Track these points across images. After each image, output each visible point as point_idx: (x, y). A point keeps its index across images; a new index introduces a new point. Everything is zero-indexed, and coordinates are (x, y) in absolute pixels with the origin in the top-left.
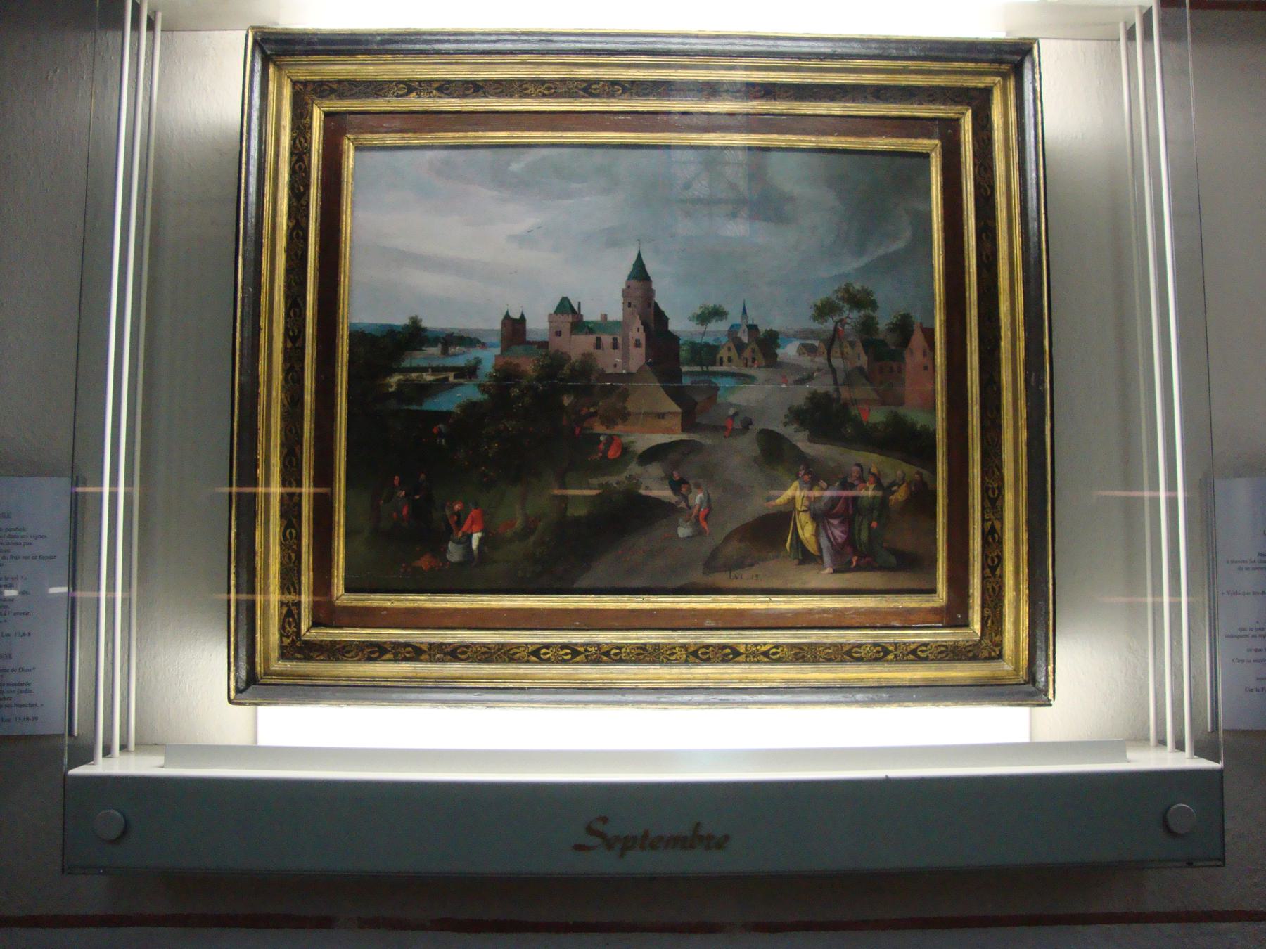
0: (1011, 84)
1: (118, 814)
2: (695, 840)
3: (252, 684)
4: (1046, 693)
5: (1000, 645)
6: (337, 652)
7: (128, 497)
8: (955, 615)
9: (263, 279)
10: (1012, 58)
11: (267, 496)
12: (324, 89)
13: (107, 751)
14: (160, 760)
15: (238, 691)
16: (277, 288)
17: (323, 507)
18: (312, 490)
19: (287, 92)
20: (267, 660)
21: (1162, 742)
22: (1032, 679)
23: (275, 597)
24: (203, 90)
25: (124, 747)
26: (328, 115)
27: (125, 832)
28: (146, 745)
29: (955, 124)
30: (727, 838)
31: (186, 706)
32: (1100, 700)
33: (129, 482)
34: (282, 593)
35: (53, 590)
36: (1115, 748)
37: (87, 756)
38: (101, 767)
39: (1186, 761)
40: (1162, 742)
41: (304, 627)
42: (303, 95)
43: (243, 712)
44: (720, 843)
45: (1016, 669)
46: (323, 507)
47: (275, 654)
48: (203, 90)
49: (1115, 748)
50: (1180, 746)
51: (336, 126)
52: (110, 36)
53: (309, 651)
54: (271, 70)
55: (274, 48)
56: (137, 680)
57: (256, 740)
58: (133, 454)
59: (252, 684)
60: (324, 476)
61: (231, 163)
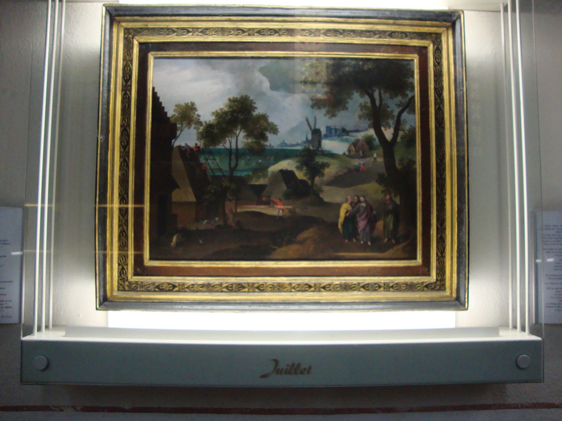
0: (450, 32)
1: (45, 358)
2: (295, 369)
3: (105, 302)
4: (464, 306)
5: (444, 285)
6: (146, 288)
7: (50, 209)
8: (425, 270)
9: (108, 244)
10: (449, 20)
11: (112, 209)
12: (138, 31)
13: (39, 329)
14: (64, 333)
15: (101, 304)
16: (115, 155)
17: (139, 213)
18: (133, 206)
19: (122, 35)
20: (112, 290)
21: (515, 327)
22: (458, 299)
23: (116, 205)
24: (81, 31)
25: (47, 327)
26: (141, 44)
27: (47, 367)
28: (56, 326)
29: (425, 48)
30: (310, 368)
31: (73, 307)
32: (489, 308)
33: (50, 202)
34: (120, 203)
35: (14, 253)
36: (494, 330)
37: (29, 330)
38: (36, 336)
39: (526, 336)
40: (515, 327)
41: (129, 277)
42: (129, 34)
43: (102, 313)
44: (309, 370)
45: (451, 293)
46: (139, 213)
47: (115, 288)
48: (81, 31)
49: (494, 330)
50: (523, 329)
51: (145, 48)
52: (44, 4)
53: (134, 287)
54: (115, 30)
55: (115, 14)
56: (53, 299)
57: (107, 324)
58: (54, 148)
59: (105, 302)
60: (139, 199)
61: (96, 67)
